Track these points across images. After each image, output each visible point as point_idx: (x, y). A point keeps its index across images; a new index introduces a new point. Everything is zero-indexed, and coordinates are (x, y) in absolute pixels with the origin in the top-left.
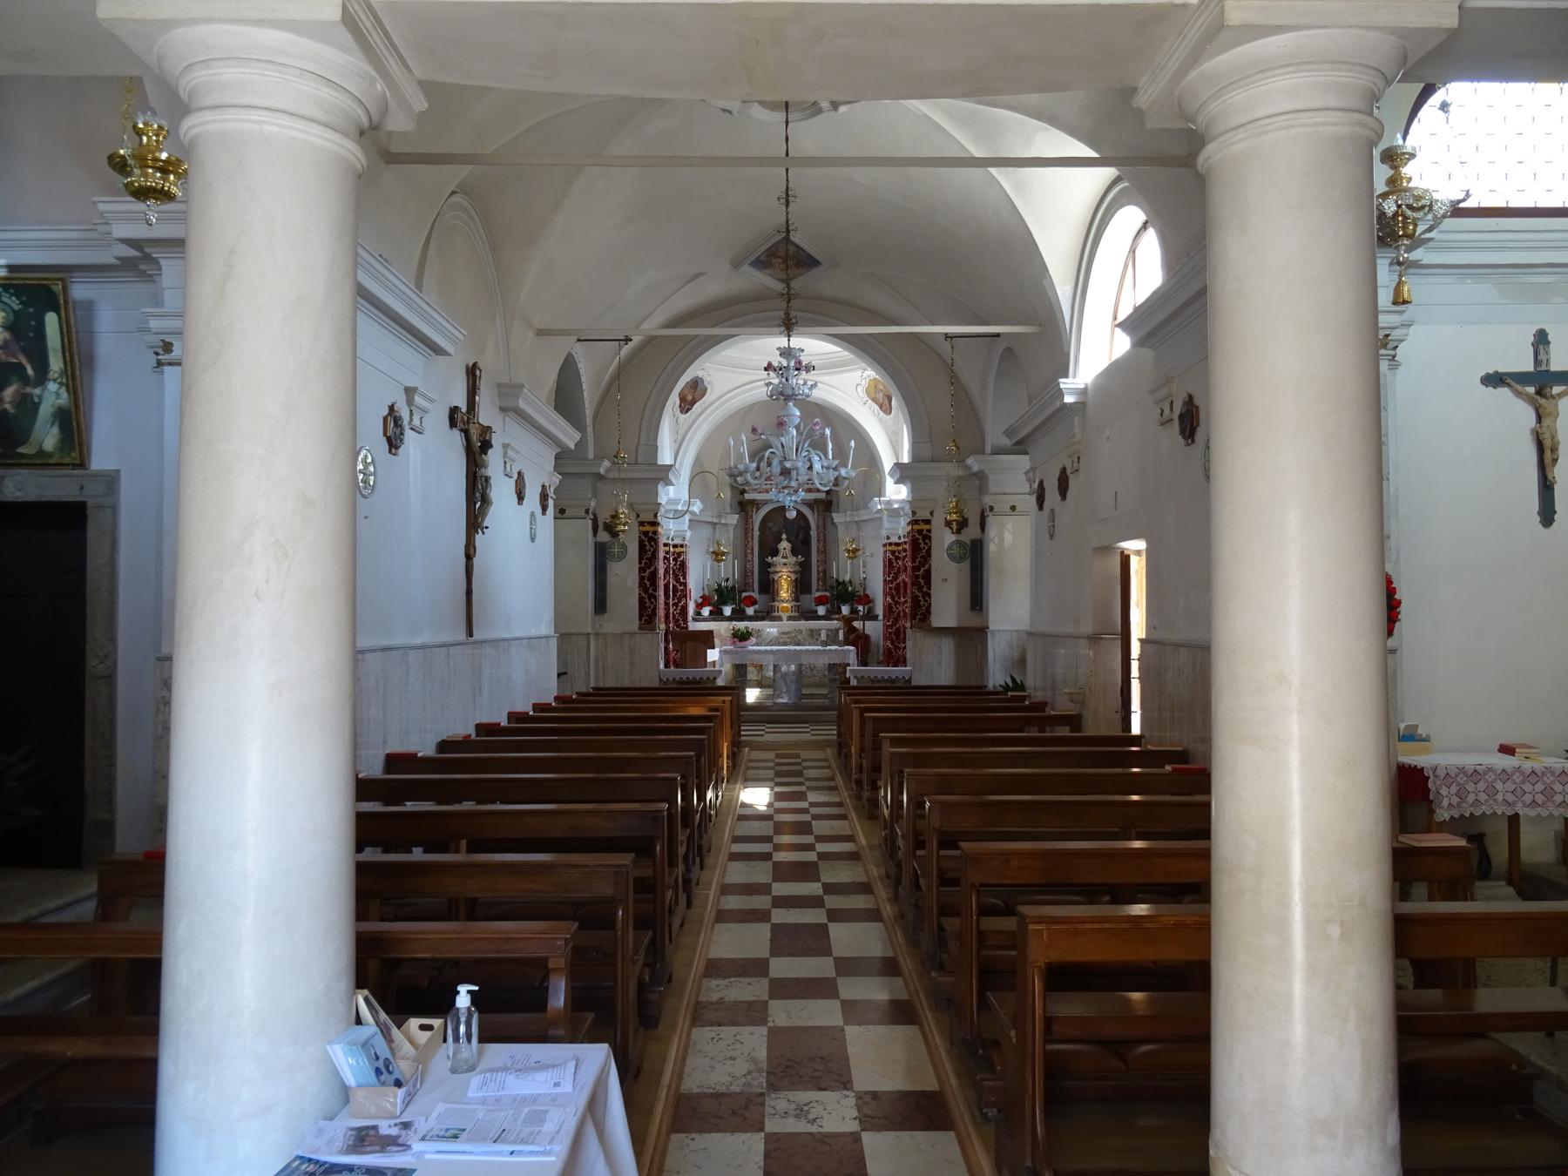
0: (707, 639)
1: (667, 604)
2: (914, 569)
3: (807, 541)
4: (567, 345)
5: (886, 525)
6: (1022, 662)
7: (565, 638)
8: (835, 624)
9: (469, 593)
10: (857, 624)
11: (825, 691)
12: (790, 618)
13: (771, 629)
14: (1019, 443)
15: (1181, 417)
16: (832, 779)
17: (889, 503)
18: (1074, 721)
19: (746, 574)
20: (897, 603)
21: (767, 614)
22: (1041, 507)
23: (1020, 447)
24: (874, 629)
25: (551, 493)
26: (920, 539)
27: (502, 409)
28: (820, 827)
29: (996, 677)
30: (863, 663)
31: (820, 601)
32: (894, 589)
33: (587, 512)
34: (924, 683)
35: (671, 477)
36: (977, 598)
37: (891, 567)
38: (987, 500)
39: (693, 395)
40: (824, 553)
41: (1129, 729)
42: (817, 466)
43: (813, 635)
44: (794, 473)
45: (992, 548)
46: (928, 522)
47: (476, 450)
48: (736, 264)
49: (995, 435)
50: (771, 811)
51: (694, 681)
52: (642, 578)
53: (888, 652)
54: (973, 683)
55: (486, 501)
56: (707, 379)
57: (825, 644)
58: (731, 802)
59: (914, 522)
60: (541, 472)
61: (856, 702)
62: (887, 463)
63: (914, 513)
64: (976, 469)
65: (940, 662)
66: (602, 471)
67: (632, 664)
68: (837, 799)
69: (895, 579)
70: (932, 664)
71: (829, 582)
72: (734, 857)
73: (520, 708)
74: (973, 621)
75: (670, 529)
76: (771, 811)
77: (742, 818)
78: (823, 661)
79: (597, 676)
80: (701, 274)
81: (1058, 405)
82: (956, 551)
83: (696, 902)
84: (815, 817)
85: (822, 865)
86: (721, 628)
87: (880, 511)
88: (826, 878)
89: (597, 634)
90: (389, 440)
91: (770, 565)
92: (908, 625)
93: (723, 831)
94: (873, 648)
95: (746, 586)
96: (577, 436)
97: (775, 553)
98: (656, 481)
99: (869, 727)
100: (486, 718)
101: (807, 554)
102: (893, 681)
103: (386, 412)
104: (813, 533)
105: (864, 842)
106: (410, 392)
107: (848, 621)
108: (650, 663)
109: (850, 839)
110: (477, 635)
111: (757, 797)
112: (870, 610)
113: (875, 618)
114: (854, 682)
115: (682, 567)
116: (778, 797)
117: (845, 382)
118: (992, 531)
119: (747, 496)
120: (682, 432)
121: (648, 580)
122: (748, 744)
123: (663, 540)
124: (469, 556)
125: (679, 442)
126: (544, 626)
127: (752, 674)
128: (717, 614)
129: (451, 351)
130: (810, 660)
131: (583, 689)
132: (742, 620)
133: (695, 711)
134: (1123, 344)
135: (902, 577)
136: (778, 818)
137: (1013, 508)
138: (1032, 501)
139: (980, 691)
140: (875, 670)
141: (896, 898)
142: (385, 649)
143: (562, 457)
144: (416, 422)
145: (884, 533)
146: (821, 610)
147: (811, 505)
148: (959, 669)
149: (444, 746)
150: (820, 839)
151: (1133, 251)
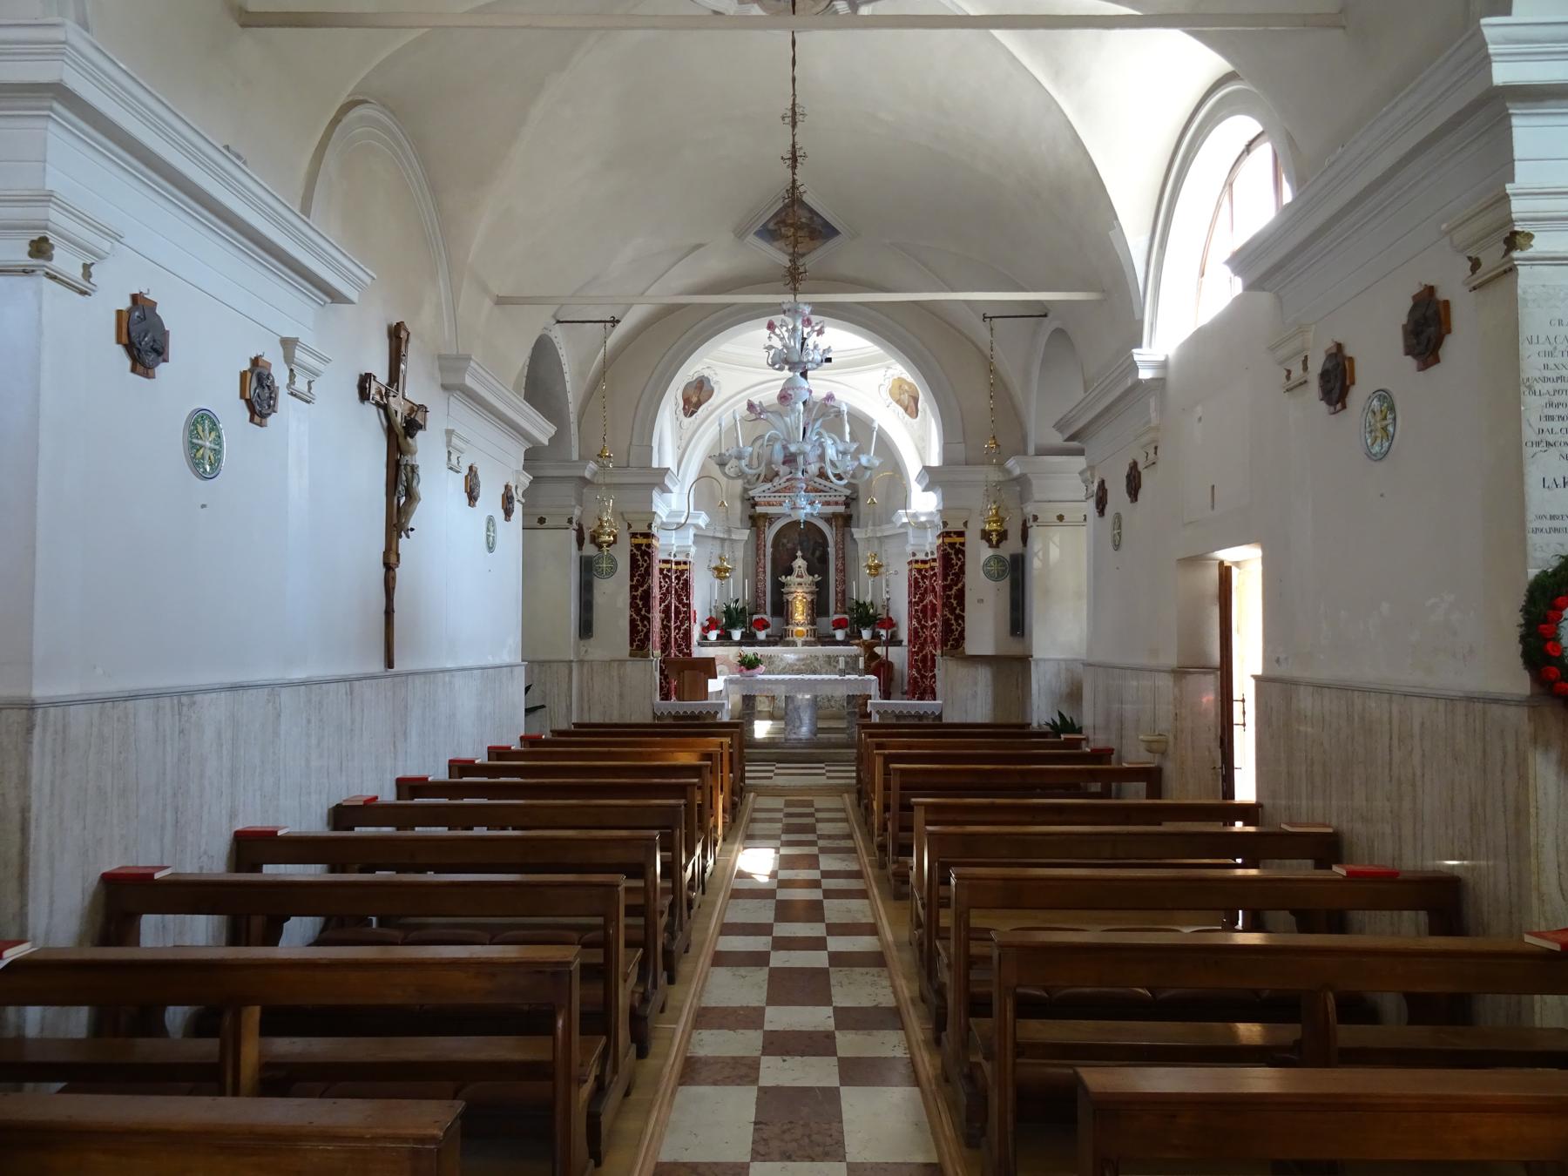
0: (708, 668)
1: (666, 628)
2: (945, 588)
3: (824, 559)
4: (537, 322)
5: (911, 540)
6: (1074, 695)
7: (537, 667)
8: (854, 650)
9: (389, 612)
10: (879, 650)
11: (842, 724)
12: (805, 643)
13: (787, 655)
14: (1072, 438)
15: (1325, 376)
16: (850, 836)
17: (915, 515)
18: (1152, 777)
19: (757, 593)
20: (923, 627)
21: (780, 639)
22: (1101, 512)
23: (1076, 441)
24: (898, 656)
25: (518, 495)
26: (952, 554)
27: (445, 387)
28: (836, 910)
29: (1041, 713)
30: (886, 695)
31: (839, 624)
32: (921, 611)
33: (570, 521)
34: (956, 721)
35: (667, 481)
36: (1018, 623)
37: (917, 586)
38: (1030, 509)
39: (697, 396)
40: (842, 570)
41: (1229, 791)
42: (831, 453)
43: (831, 661)
44: (800, 459)
45: (1035, 564)
47: (401, 435)
48: (740, 234)
49: (1042, 431)
50: (774, 886)
51: (693, 716)
52: (633, 598)
53: (914, 682)
54: (1014, 721)
55: (411, 495)
56: (713, 379)
57: (843, 672)
58: (724, 867)
59: (946, 534)
60: (503, 468)
61: (880, 746)
62: (913, 468)
63: (945, 524)
64: (1017, 472)
65: (975, 696)
66: (587, 475)
67: (621, 696)
68: (855, 867)
69: (921, 600)
70: (965, 697)
71: (848, 604)
72: (720, 959)
73: (466, 755)
74: (1014, 648)
75: (668, 545)
76: (774, 886)
77: (736, 894)
78: (841, 692)
79: (581, 710)
80: (699, 246)
81: (1129, 382)
82: (994, 567)
83: (655, 1048)
84: (829, 894)
85: (836, 976)
86: (726, 655)
87: (904, 525)
88: (841, 998)
89: (581, 662)
90: (250, 404)
91: (783, 585)
92: (939, 652)
93: (710, 916)
94: (897, 676)
95: (758, 608)
96: (551, 429)
97: (790, 571)
98: (650, 486)
99: (895, 782)
100: (413, 771)
101: (824, 572)
102: (920, 717)
103: (247, 366)
104: (831, 550)
105: (889, 937)
106: (288, 344)
107: (869, 647)
108: (637, 694)
109: (873, 930)
110: (397, 667)
111: (757, 862)
112: (894, 635)
113: (899, 643)
114: (875, 719)
115: (686, 586)
116: (786, 862)
117: (864, 378)
118: (1036, 544)
119: (759, 509)
120: (686, 437)
121: (640, 601)
122: (754, 788)
123: (660, 555)
124: (389, 567)
125: (680, 447)
126: (509, 651)
127: (762, 705)
128: (725, 639)
129: (352, 294)
130: (827, 691)
131: (563, 725)
132: (752, 645)
133: (686, 758)
134: (1237, 286)
135: (930, 598)
136: (783, 894)
137: (1061, 518)
138: (1091, 505)
139: (1021, 730)
140: (900, 703)
141: (936, 1042)
142: (233, 688)
143: (533, 457)
144: (301, 384)
145: (909, 549)
147: (828, 519)
148: (998, 701)
149: (342, 815)
150: (834, 930)
151: (1229, 184)
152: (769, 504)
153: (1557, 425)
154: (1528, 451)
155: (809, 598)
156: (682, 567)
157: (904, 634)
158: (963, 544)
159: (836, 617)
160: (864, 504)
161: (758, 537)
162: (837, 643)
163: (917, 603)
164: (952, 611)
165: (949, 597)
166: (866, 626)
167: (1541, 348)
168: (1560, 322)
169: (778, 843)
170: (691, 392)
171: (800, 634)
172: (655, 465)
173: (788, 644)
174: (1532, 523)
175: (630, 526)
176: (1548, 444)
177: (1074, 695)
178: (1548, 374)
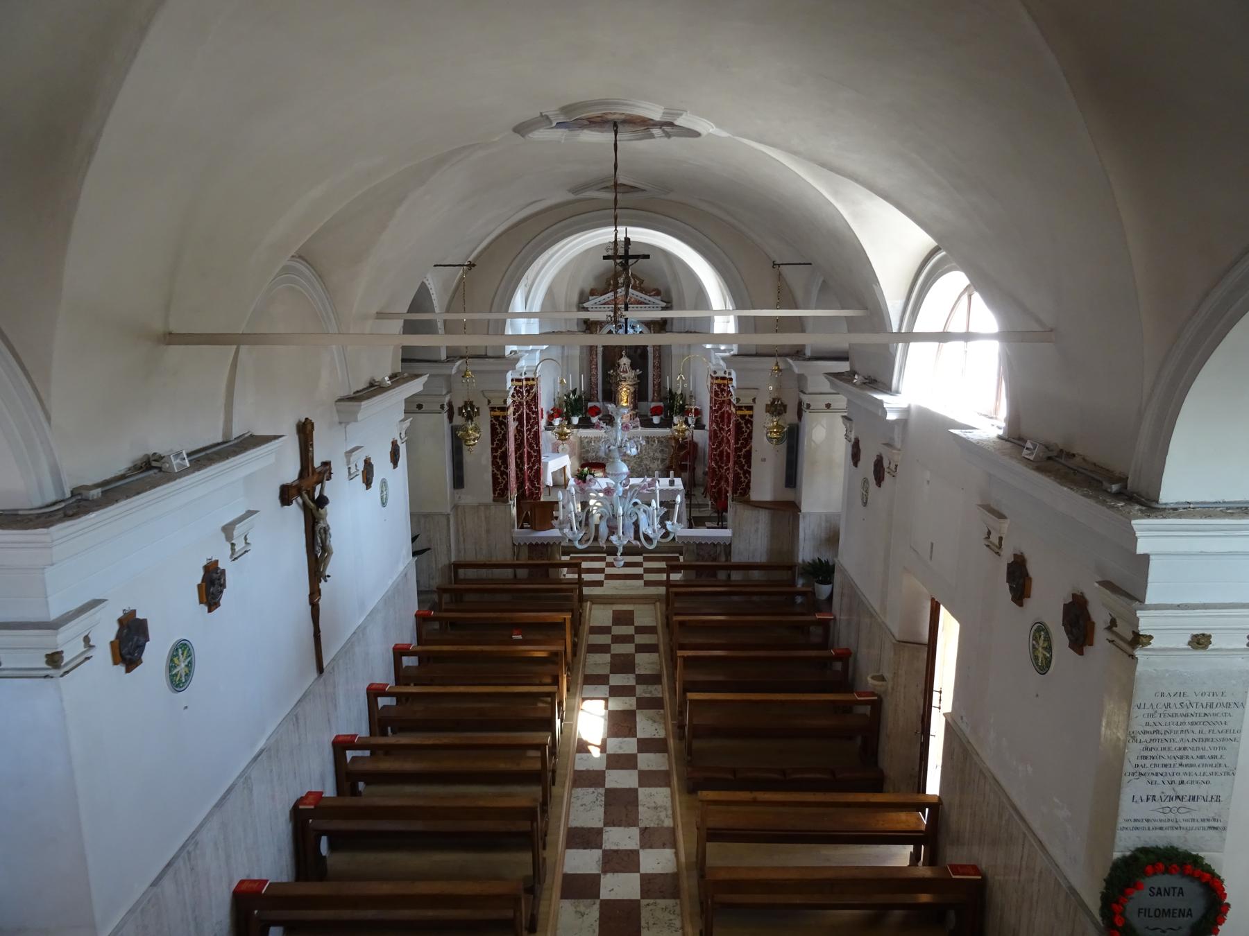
19: (591, 385)
29: (806, 552)
31: (656, 411)
33: (442, 407)
36: (791, 476)
40: (659, 368)
46: (750, 408)
52: (494, 458)
55: (326, 549)
65: (757, 531)
67: (488, 531)
71: (663, 394)
74: (788, 495)
79: (458, 551)
94: (700, 454)
101: (644, 368)
108: (504, 531)
113: (703, 427)
115: (535, 399)
137: (828, 406)
146: (656, 420)
148: (774, 536)
153: (1148, 762)
154: (1125, 779)
156: (531, 383)
157: (706, 420)
158: (751, 416)
159: (653, 405)
163: (716, 411)
164: (742, 467)
165: (739, 457)
167: (1146, 711)
168: (1162, 695)
169: (604, 690)
174: (1121, 823)
175: (489, 402)
176: (1141, 774)
177: (832, 539)
178: (1148, 729)
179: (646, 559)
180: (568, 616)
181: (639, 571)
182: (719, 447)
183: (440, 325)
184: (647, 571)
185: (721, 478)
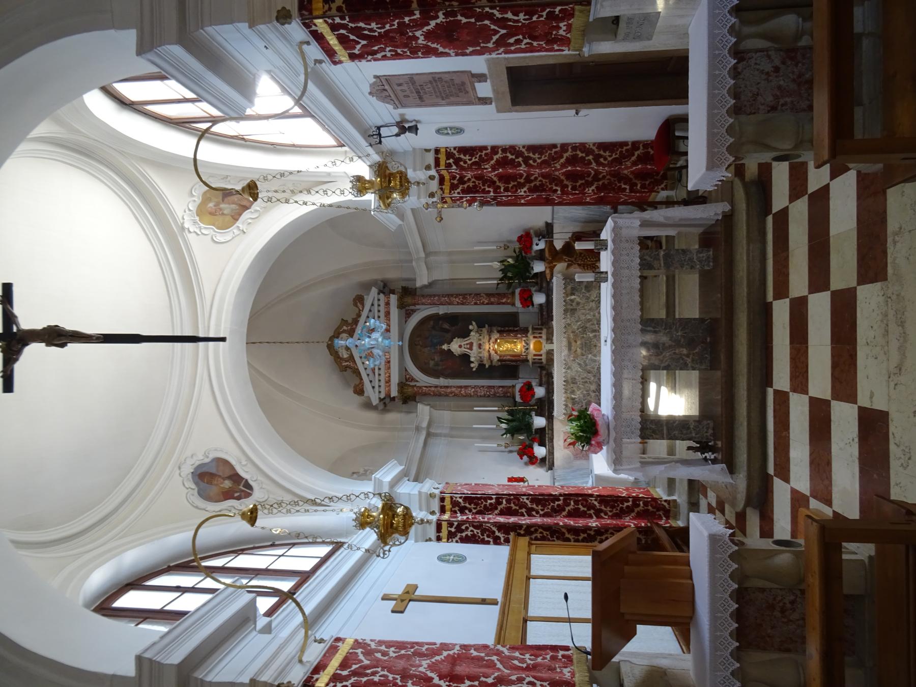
3: (452, 319)
8: (557, 283)
12: (550, 339)
19: (491, 396)
20: (528, 180)
21: (544, 370)
31: (527, 300)
40: (464, 297)
56: (200, 458)
71: (503, 289)
91: (481, 365)
95: (507, 395)
97: (465, 358)
101: (467, 318)
104: (442, 310)
119: (394, 393)
128: (544, 436)
146: (539, 299)
147: (407, 311)
152: (388, 382)
155: (496, 335)
156: (447, 503)
159: (518, 304)
160: (391, 275)
161: (425, 394)
162: (549, 302)
166: (528, 268)
170: (214, 490)
171: (538, 347)
172: (128, 669)
173: (550, 360)
179: (782, 291)
180: (417, 15)
181: (820, 308)
182: (559, 182)
183: (502, 539)
184: (819, 278)
185: (617, 175)
